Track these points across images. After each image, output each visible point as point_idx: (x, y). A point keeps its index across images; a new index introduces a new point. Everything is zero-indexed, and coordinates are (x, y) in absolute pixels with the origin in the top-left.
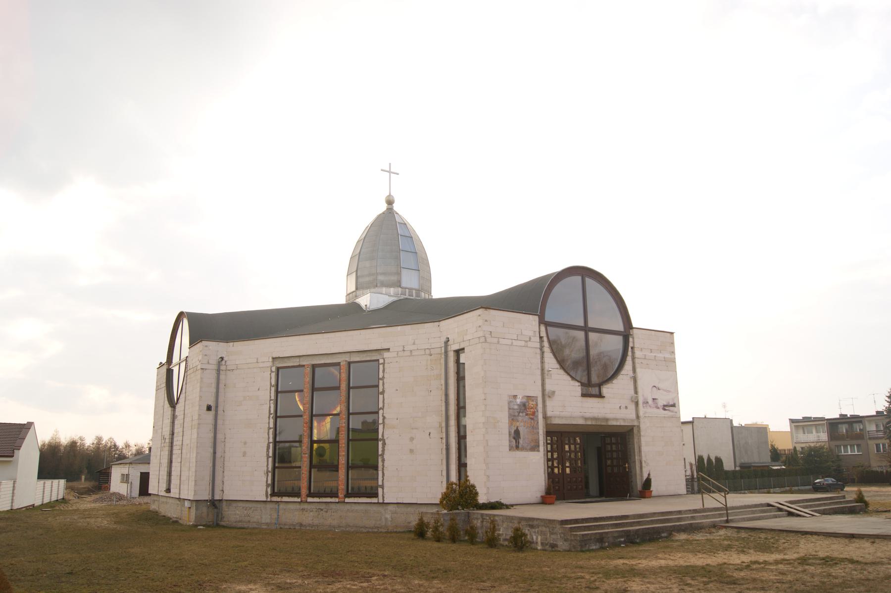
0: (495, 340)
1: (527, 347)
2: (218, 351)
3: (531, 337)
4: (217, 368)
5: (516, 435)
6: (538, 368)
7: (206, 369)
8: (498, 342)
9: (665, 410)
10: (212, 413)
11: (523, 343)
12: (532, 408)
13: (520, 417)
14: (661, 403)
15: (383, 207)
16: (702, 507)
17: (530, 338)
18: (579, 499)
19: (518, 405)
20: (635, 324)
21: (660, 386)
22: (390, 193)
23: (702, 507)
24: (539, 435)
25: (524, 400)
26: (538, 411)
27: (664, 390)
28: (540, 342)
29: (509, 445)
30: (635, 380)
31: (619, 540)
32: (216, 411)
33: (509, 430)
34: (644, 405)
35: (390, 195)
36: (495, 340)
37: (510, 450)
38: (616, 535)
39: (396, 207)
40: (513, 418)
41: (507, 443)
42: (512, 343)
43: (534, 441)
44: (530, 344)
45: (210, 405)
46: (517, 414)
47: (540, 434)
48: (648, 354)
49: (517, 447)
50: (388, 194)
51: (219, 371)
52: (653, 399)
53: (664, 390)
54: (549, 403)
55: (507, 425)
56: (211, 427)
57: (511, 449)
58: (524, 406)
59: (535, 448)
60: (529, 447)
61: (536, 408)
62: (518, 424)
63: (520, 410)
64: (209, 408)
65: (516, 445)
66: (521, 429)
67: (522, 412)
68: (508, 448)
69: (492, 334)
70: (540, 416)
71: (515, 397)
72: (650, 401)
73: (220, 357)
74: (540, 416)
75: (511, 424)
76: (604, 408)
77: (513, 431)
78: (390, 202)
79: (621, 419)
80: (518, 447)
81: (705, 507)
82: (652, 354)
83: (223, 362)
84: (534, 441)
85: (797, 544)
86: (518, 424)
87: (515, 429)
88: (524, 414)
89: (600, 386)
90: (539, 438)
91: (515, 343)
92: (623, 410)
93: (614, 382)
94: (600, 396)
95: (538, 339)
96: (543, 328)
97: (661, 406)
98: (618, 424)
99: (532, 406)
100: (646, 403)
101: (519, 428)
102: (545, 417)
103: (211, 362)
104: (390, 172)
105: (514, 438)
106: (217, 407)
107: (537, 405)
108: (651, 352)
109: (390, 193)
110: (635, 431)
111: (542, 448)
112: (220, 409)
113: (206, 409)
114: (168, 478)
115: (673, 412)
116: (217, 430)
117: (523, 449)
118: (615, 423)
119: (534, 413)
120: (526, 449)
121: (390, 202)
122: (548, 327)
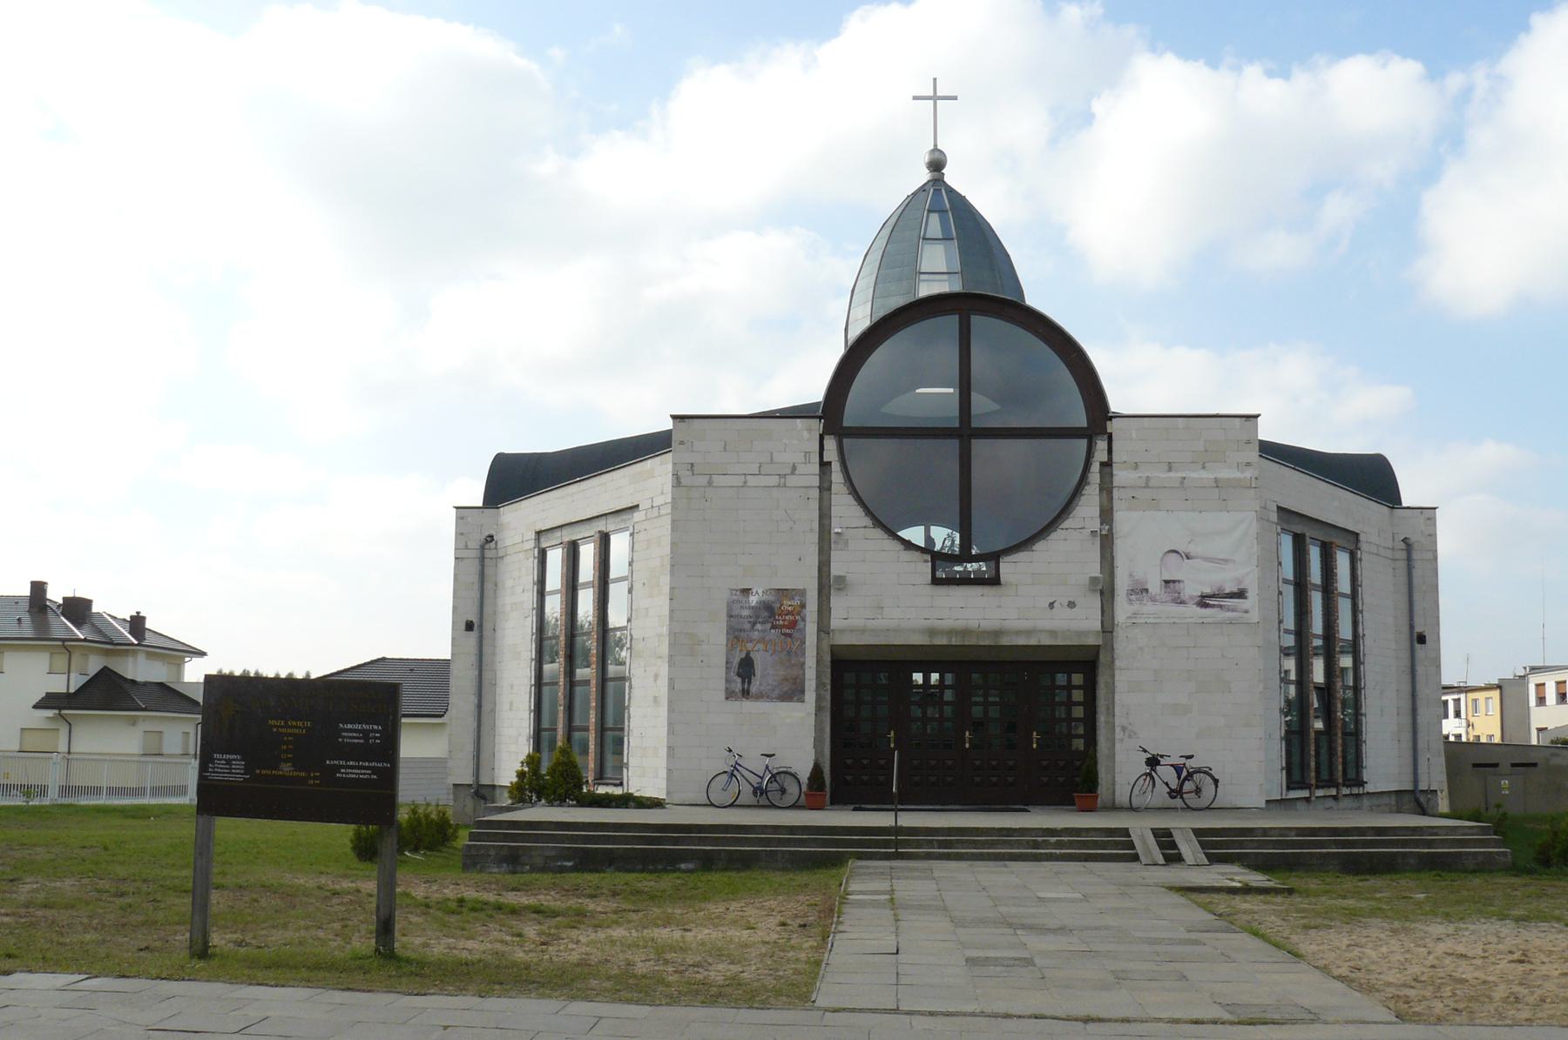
0: (703, 480)
1: (785, 486)
2: (482, 525)
3: (798, 466)
4: (479, 556)
5: (746, 669)
6: (811, 530)
7: (462, 558)
8: (710, 483)
9: (1206, 606)
10: (473, 635)
11: (774, 480)
12: (789, 613)
13: (756, 633)
14: (1192, 590)
15: (924, 176)
16: (894, 824)
17: (794, 468)
18: (931, 804)
19: (753, 607)
20: (1116, 404)
21: (1192, 549)
22: (935, 145)
23: (894, 824)
24: (804, 670)
25: (770, 598)
26: (804, 620)
27: (1206, 559)
28: (819, 475)
29: (727, 688)
30: (1107, 542)
31: (559, 864)
32: (481, 631)
33: (727, 658)
34: (1133, 597)
35: (935, 149)
36: (703, 480)
37: (727, 698)
38: (553, 853)
39: (951, 177)
40: (735, 635)
41: (722, 685)
42: (745, 482)
43: (791, 681)
44: (792, 481)
45: (472, 622)
46: (747, 626)
47: (806, 666)
48: (1159, 475)
49: (746, 693)
50: (932, 148)
51: (482, 559)
52: (1167, 582)
53: (1206, 559)
54: (837, 603)
55: (723, 650)
56: (473, 659)
57: (730, 695)
58: (768, 611)
59: (793, 692)
60: (777, 692)
61: (799, 614)
62: (749, 646)
63: (758, 617)
64: (469, 626)
65: (743, 689)
66: (759, 659)
67: (763, 623)
68: (722, 695)
69: (695, 468)
70: (811, 629)
71: (746, 591)
72: (1155, 587)
73: (487, 534)
74: (811, 629)
75: (731, 647)
76: (999, 607)
77: (736, 661)
78: (937, 165)
79: (1046, 631)
80: (748, 693)
81: (899, 824)
82: (1172, 474)
83: (492, 545)
84: (791, 681)
85: (1485, 947)
86: (749, 646)
87: (743, 655)
88: (769, 625)
89: (994, 557)
90: (804, 674)
91: (752, 481)
92: (1062, 612)
93: (1034, 548)
94: (995, 581)
95: (816, 468)
96: (831, 444)
97: (1191, 597)
98: (1033, 642)
99: (790, 608)
100: (1140, 591)
101: (751, 655)
102: (823, 628)
103: (470, 545)
104: (935, 98)
105: (739, 675)
106: (481, 626)
107: (803, 606)
108: (1170, 469)
109: (935, 145)
110: (1103, 658)
111: (810, 696)
112: (487, 626)
113: (464, 628)
114: (599, 751)
115: (1233, 610)
116: (484, 664)
117: (760, 696)
118: (1021, 641)
119: (793, 624)
120: (768, 697)
121: (937, 165)
122: (845, 440)
